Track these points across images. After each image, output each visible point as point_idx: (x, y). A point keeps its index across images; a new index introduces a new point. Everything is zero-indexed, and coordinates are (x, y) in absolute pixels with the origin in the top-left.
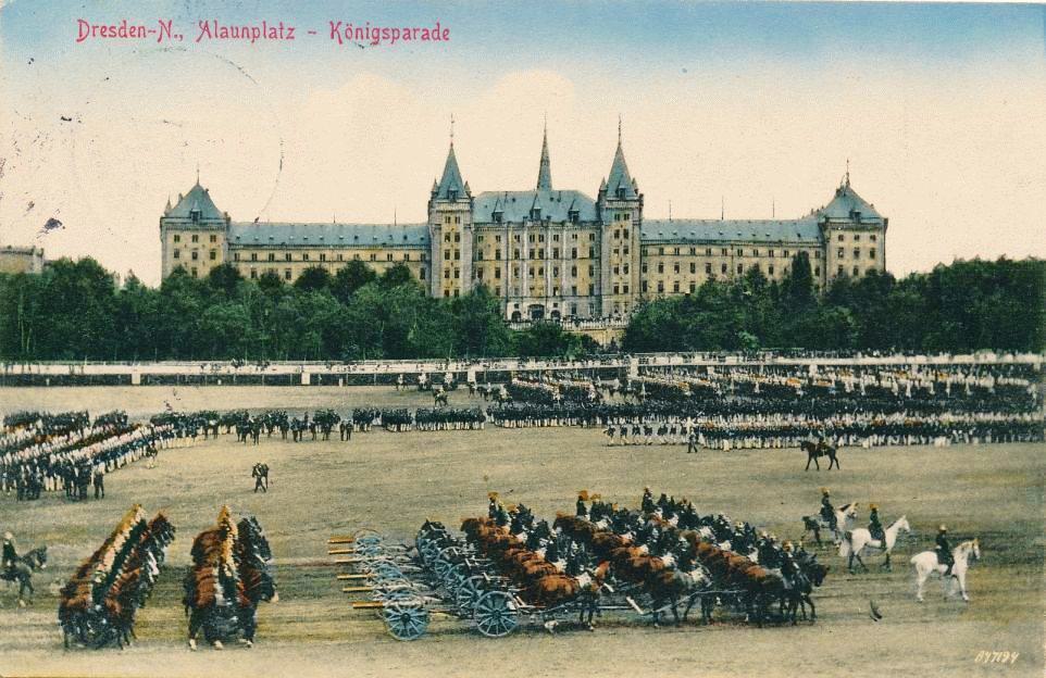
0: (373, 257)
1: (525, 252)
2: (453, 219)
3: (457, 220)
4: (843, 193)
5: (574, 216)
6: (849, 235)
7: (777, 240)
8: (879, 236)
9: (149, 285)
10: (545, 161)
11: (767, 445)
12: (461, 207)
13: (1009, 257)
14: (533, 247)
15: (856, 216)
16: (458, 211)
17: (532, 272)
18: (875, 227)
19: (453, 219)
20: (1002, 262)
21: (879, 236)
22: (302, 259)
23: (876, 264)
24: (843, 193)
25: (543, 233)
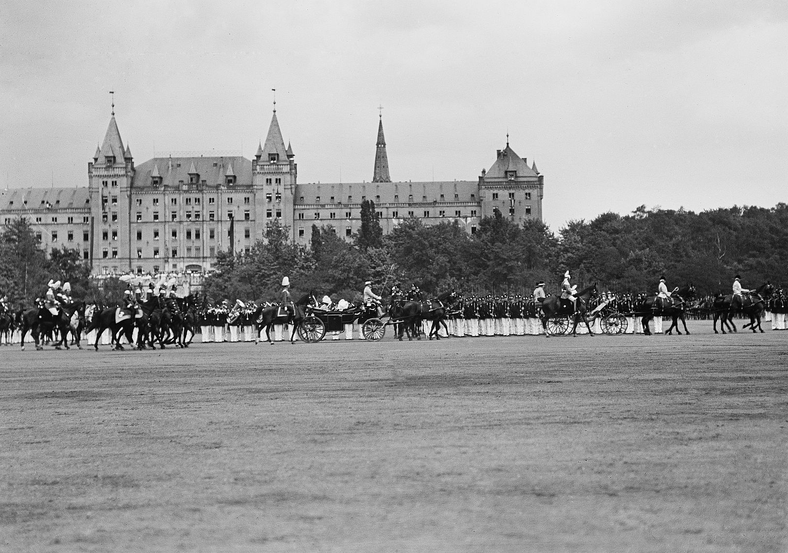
0: (426, 214)
1: (181, 214)
2: (110, 184)
3: (114, 184)
4: (505, 155)
5: (231, 181)
6: (503, 194)
7: (432, 202)
8: (534, 193)
9: (546, 220)
10: (381, 143)
11: (442, 332)
12: (117, 171)
13: (662, 209)
14: (271, 208)
15: (513, 174)
16: (115, 176)
17: (189, 234)
18: (530, 185)
19: (110, 184)
20: (720, 210)
21: (534, 193)
22: (67, 221)
23: (533, 217)
24: (505, 155)
25: (199, 196)
